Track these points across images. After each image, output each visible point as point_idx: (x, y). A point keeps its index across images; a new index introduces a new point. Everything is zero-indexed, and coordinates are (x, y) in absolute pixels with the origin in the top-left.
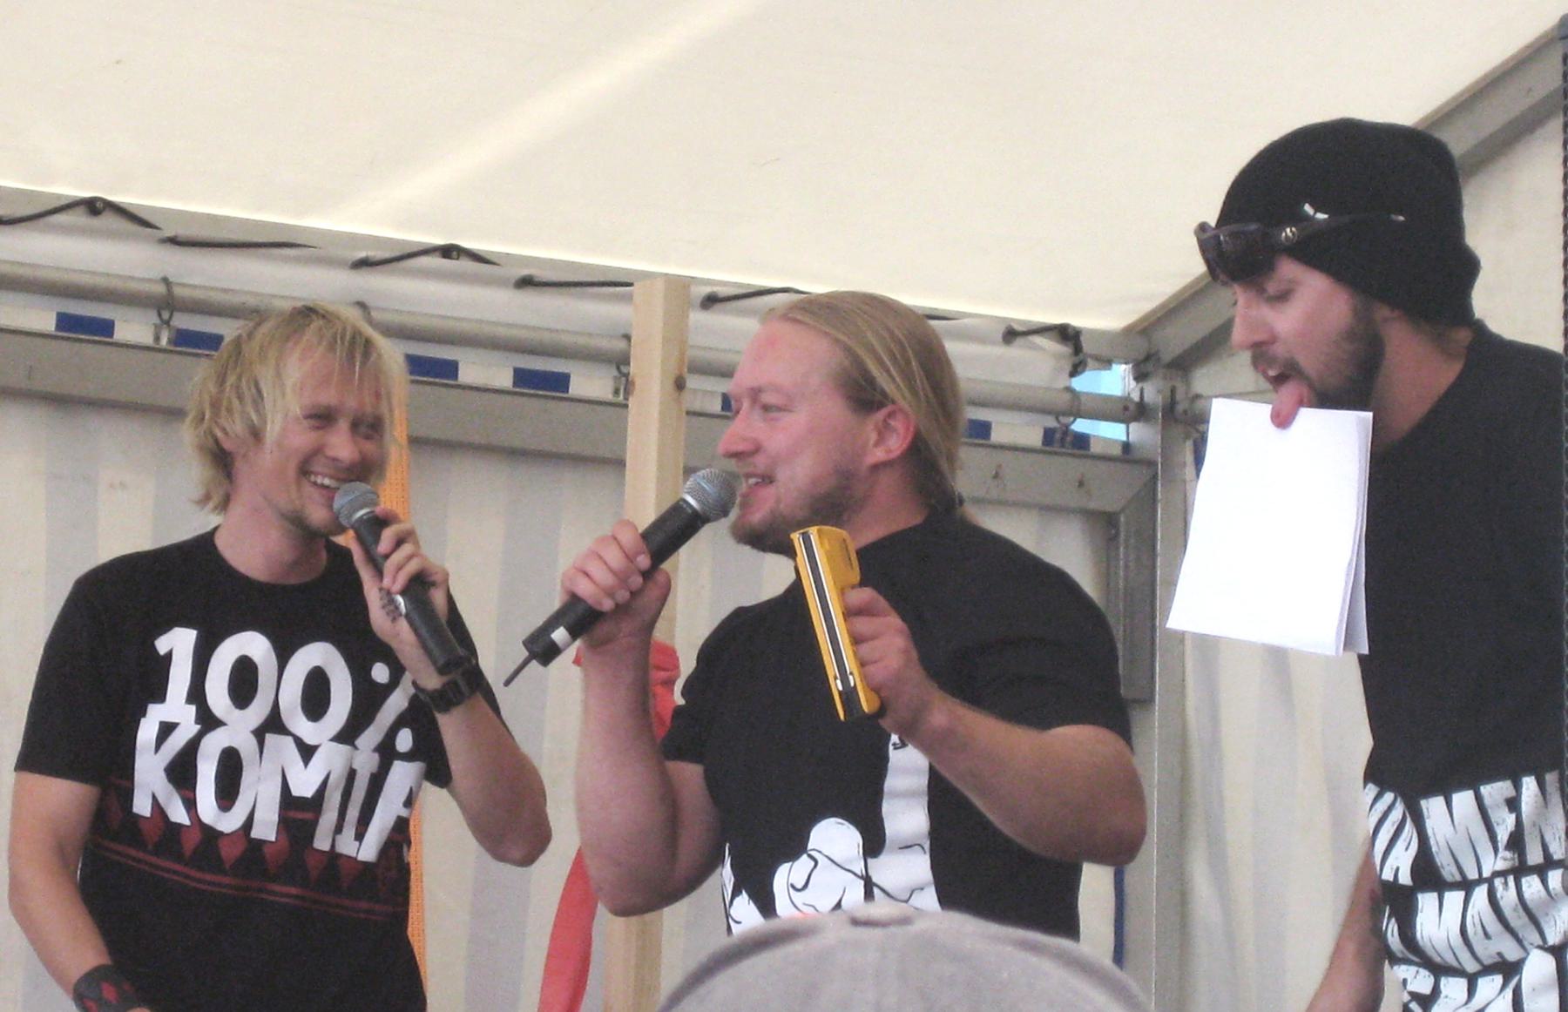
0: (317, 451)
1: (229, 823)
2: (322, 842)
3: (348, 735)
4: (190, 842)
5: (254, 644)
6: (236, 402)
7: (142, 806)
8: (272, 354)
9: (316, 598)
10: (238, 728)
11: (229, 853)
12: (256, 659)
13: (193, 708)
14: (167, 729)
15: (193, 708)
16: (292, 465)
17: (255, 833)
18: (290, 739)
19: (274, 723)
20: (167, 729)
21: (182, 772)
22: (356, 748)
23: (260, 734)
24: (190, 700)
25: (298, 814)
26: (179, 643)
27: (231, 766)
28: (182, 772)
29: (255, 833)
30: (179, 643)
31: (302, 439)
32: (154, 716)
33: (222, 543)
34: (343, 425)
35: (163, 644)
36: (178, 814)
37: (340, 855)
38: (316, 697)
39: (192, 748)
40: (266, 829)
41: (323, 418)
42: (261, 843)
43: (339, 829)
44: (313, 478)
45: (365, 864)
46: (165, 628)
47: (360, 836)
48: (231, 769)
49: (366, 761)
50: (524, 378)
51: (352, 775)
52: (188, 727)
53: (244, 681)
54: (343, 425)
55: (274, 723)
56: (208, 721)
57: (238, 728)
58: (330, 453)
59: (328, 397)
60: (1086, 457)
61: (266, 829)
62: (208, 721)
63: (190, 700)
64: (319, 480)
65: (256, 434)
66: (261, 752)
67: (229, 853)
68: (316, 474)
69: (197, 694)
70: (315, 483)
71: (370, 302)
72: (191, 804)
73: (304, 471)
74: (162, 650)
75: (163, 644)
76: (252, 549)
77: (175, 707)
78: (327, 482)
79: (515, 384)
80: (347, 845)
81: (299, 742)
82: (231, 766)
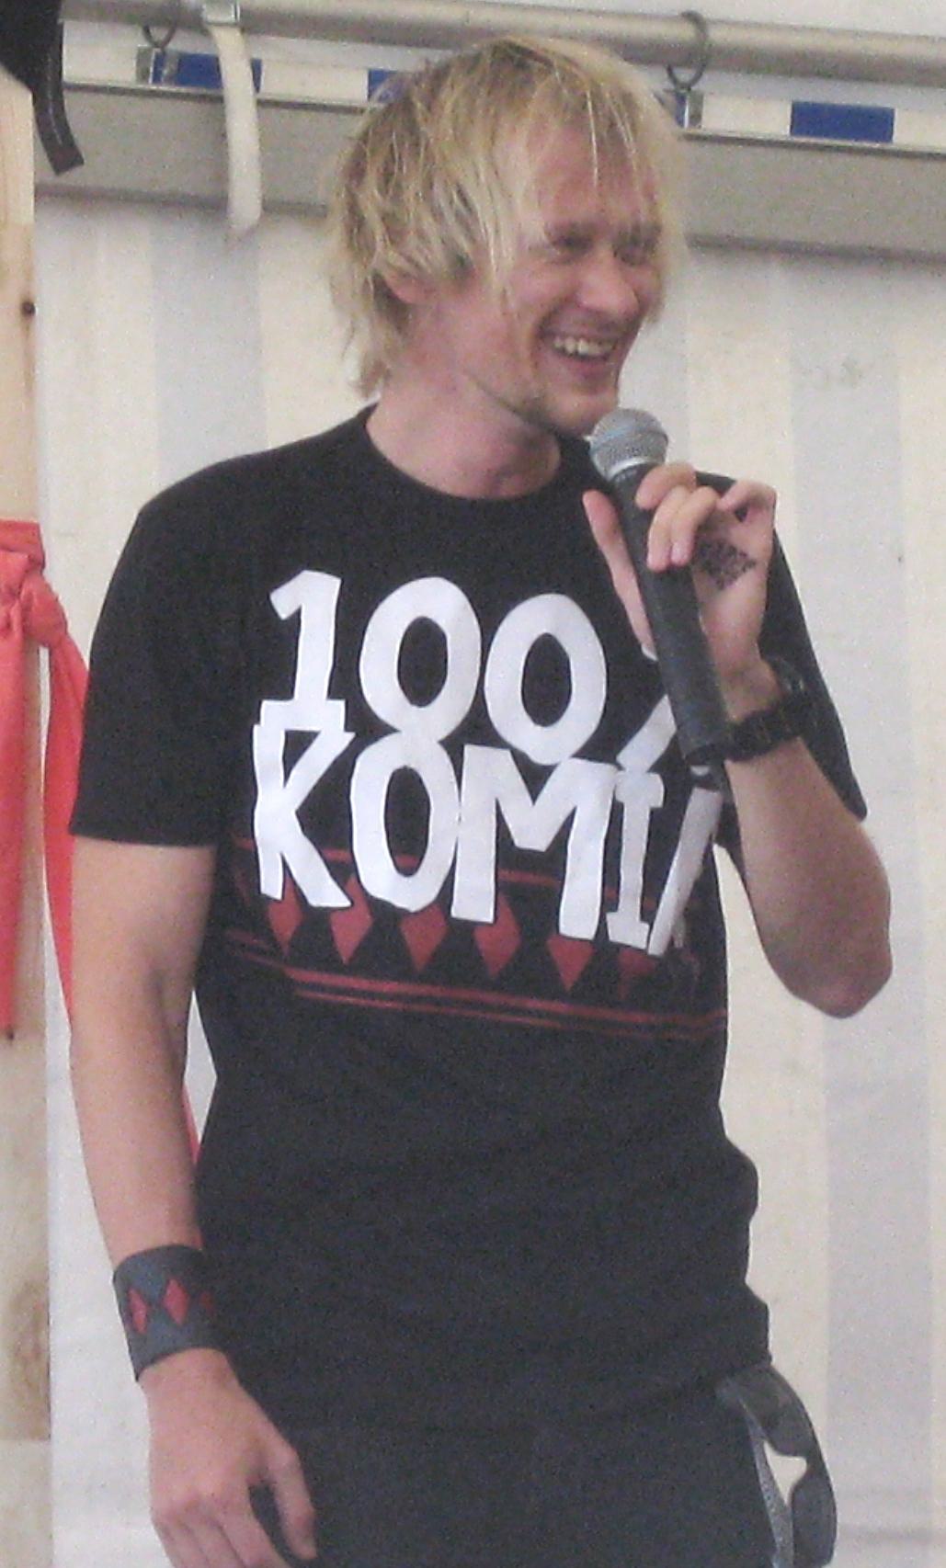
0: (569, 299)
1: (411, 894)
2: (577, 914)
3: (603, 747)
4: (347, 940)
5: (435, 599)
6: (427, 221)
7: (271, 885)
8: (478, 140)
9: (528, 528)
10: (416, 736)
11: (420, 945)
12: (443, 623)
13: (341, 704)
14: (297, 744)
15: (341, 704)
16: (526, 328)
17: (459, 910)
18: (507, 754)
19: (476, 728)
20: (297, 744)
21: (326, 817)
22: (620, 768)
23: (454, 746)
24: (333, 693)
25: (529, 877)
26: (310, 598)
27: (407, 802)
28: (326, 817)
29: (459, 910)
30: (310, 598)
31: (545, 283)
32: (272, 723)
33: (384, 437)
34: (604, 252)
35: (284, 601)
36: (325, 893)
37: (619, 947)
38: (546, 684)
39: (341, 771)
40: (476, 901)
41: (572, 243)
42: (469, 927)
43: (610, 901)
44: (558, 343)
45: (653, 957)
46: (284, 574)
47: (648, 914)
48: (408, 809)
49: (644, 794)
50: (807, 119)
51: (617, 812)
52: (333, 738)
53: (423, 662)
54: (604, 252)
55: (476, 728)
56: (366, 727)
57: (416, 736)
58: (588, 300)
59: (583, 210)
60: (883, 153)
61: (476, 901)
62: (366, 727)
63: (333, 693)
64: (570, 347)
65: (464, 272)
66: (498, 807)
67: (420, 945)
68: (564, 336)
69: (344, 682)
70: (563, 351)
71: (707, 13)
72: (344, 871)
73: (545, 332)
74: (284, 612)
75: (284, 601)
76: (440, 448)
77: (310, 705)
78: (583, 347)
79: (143, 75)
80: (627, 929)
81: (521, 760)
82: (407, 802)
